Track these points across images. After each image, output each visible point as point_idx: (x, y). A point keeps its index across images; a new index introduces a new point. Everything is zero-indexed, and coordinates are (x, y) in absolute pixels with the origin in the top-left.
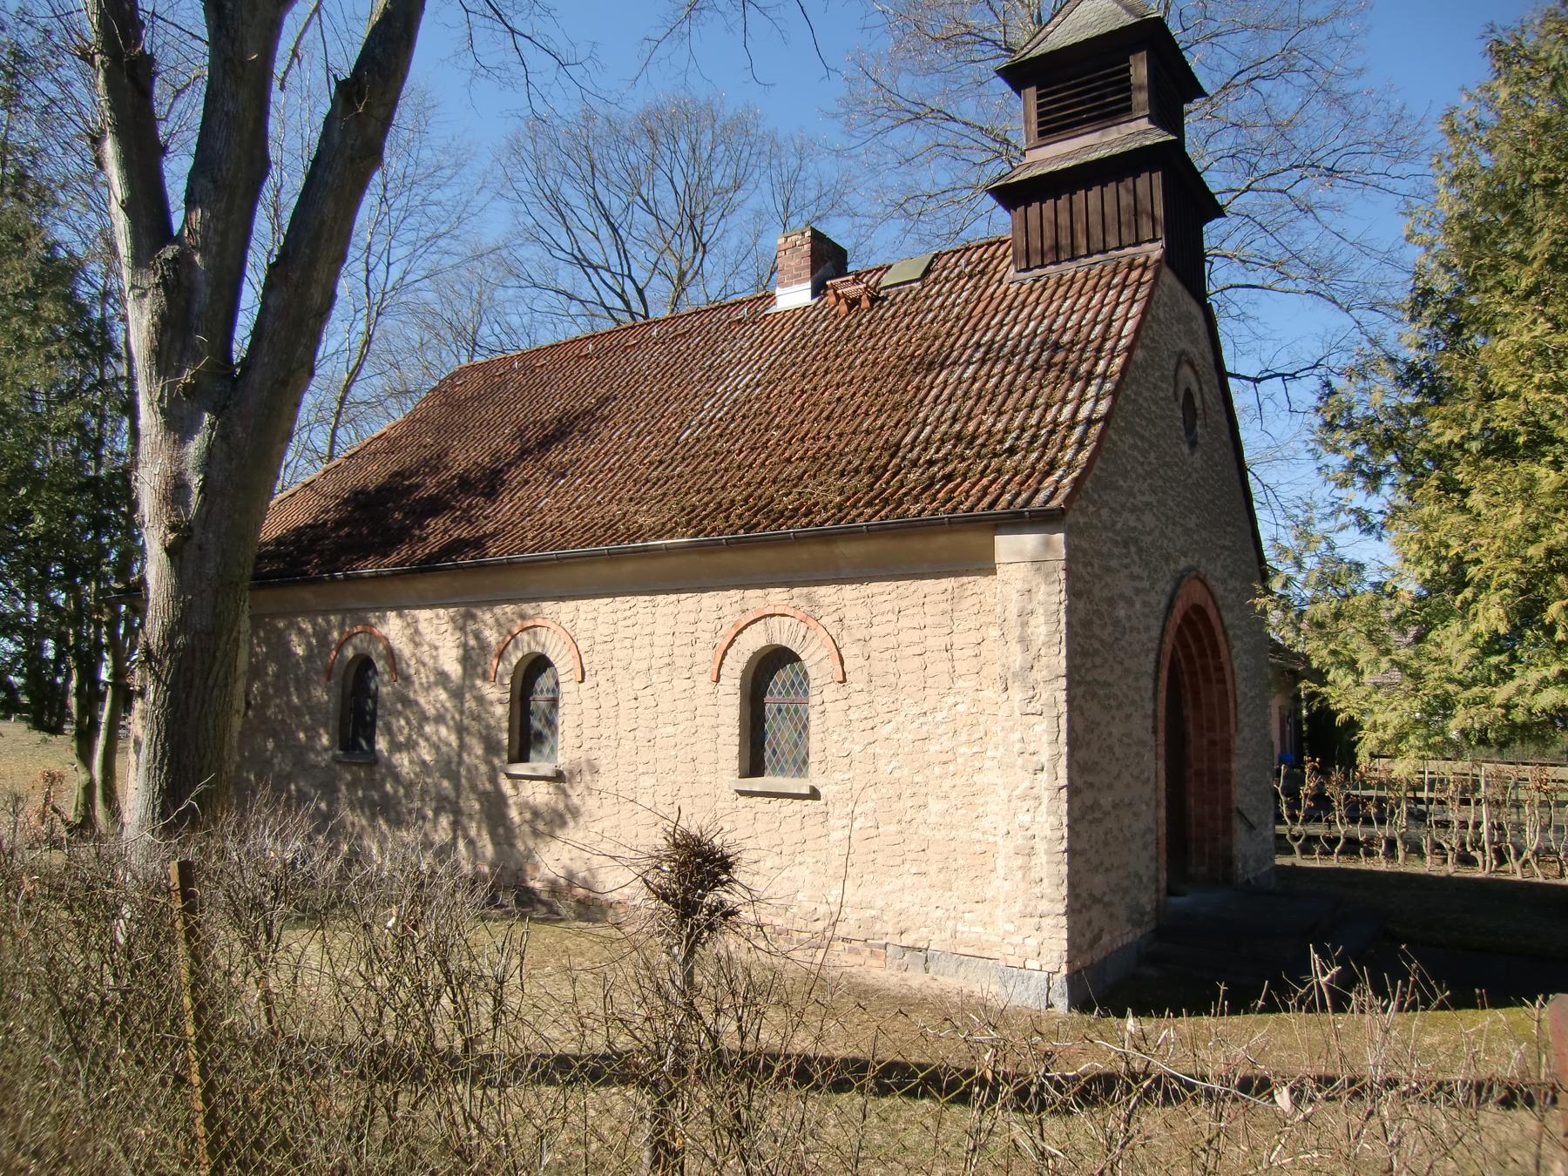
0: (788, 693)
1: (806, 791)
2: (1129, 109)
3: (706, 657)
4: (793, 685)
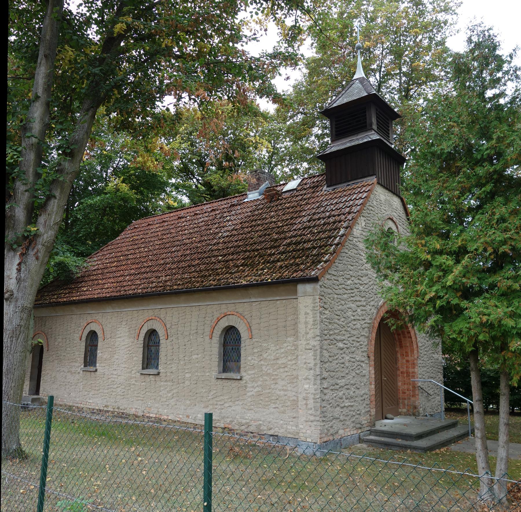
0: (235, 343)
1: (239, 378)
2: (366, 126)
3: (208, 330)
4: (237, 340)
